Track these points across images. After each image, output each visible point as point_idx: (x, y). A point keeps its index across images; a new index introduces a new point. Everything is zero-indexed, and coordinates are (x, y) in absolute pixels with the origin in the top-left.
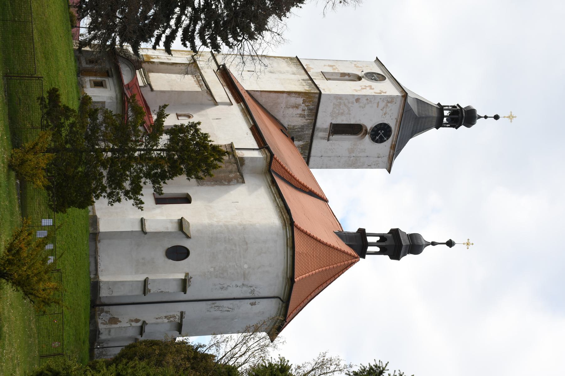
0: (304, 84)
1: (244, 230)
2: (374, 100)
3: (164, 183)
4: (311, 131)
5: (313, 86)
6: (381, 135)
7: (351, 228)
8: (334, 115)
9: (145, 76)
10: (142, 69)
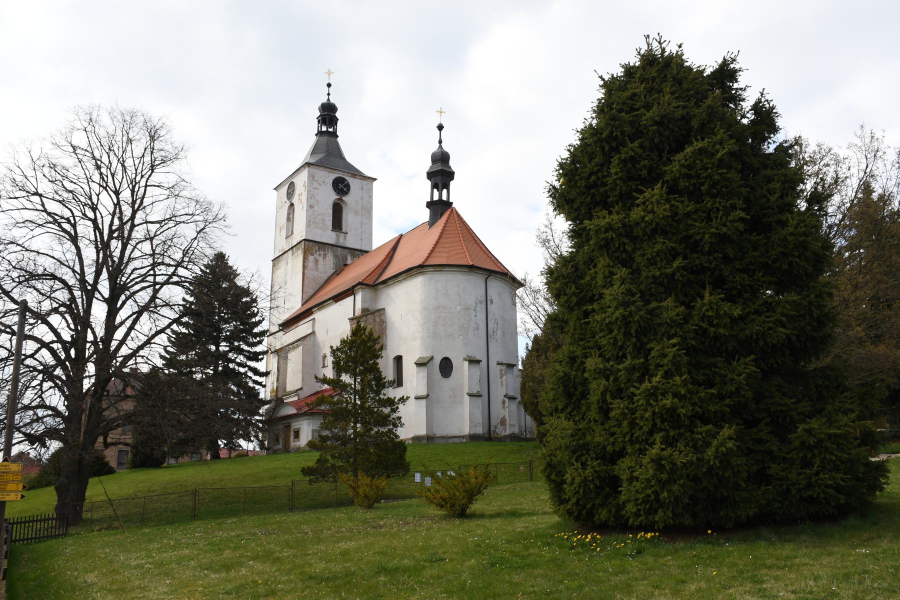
3: (385, 378)
7: (425, 215)
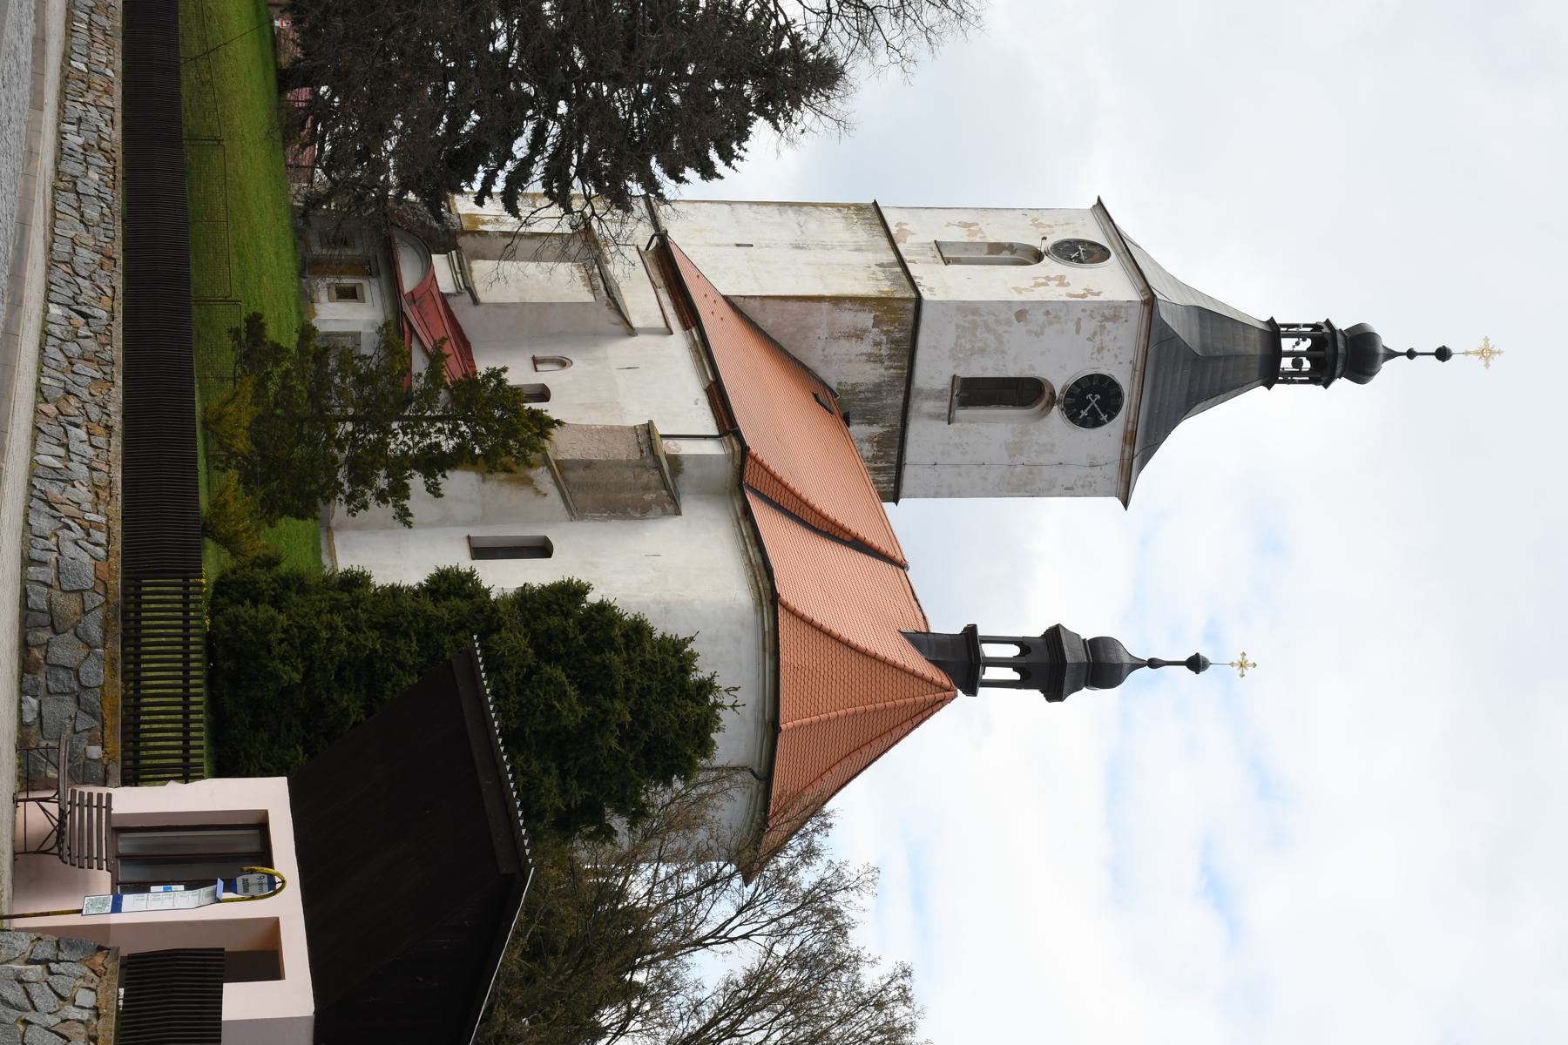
0: (881, 276)
1: (666, 613)
2: (1066, 315)
3: (444, 476)
4: (901, 397)
5: (904, 281)
6: (1093, 406)
7: (946, 623)
8: (961, 355)
9: (460, 268)
10: (454, 252)
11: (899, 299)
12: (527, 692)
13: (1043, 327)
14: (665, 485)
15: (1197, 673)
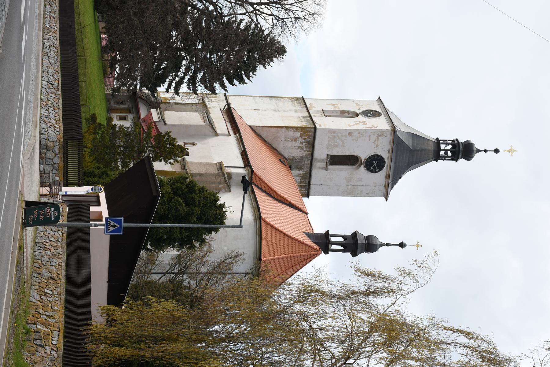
0: (303, 120)
2: (365, 134)
4: (310, 161)
5: (311, 122)
6: (375, 166)
7: (319, 230)
8: (330, 147)
11: (308, 128)
12: (170, 204)
13: (358, 138)
14: (226, 182)
15: (402, 248)
